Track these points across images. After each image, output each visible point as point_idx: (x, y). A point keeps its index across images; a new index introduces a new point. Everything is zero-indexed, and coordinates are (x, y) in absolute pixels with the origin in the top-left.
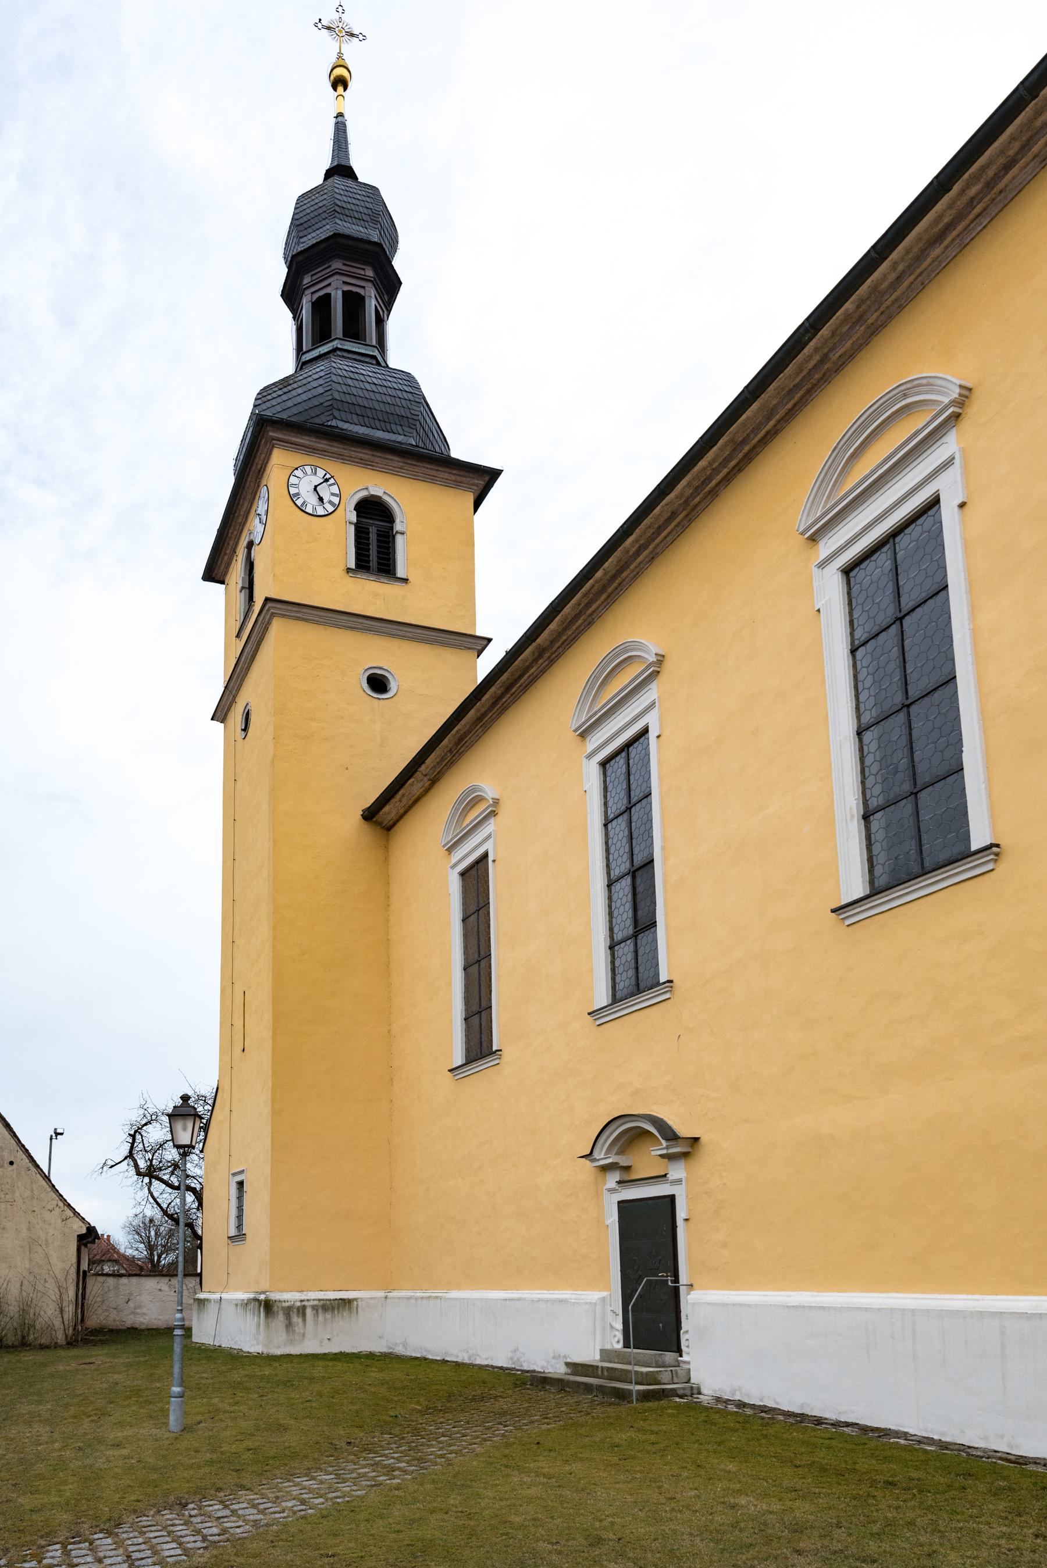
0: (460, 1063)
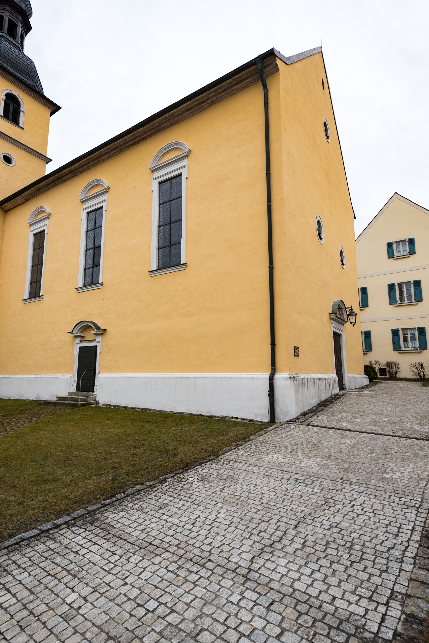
0: (27, 298)
